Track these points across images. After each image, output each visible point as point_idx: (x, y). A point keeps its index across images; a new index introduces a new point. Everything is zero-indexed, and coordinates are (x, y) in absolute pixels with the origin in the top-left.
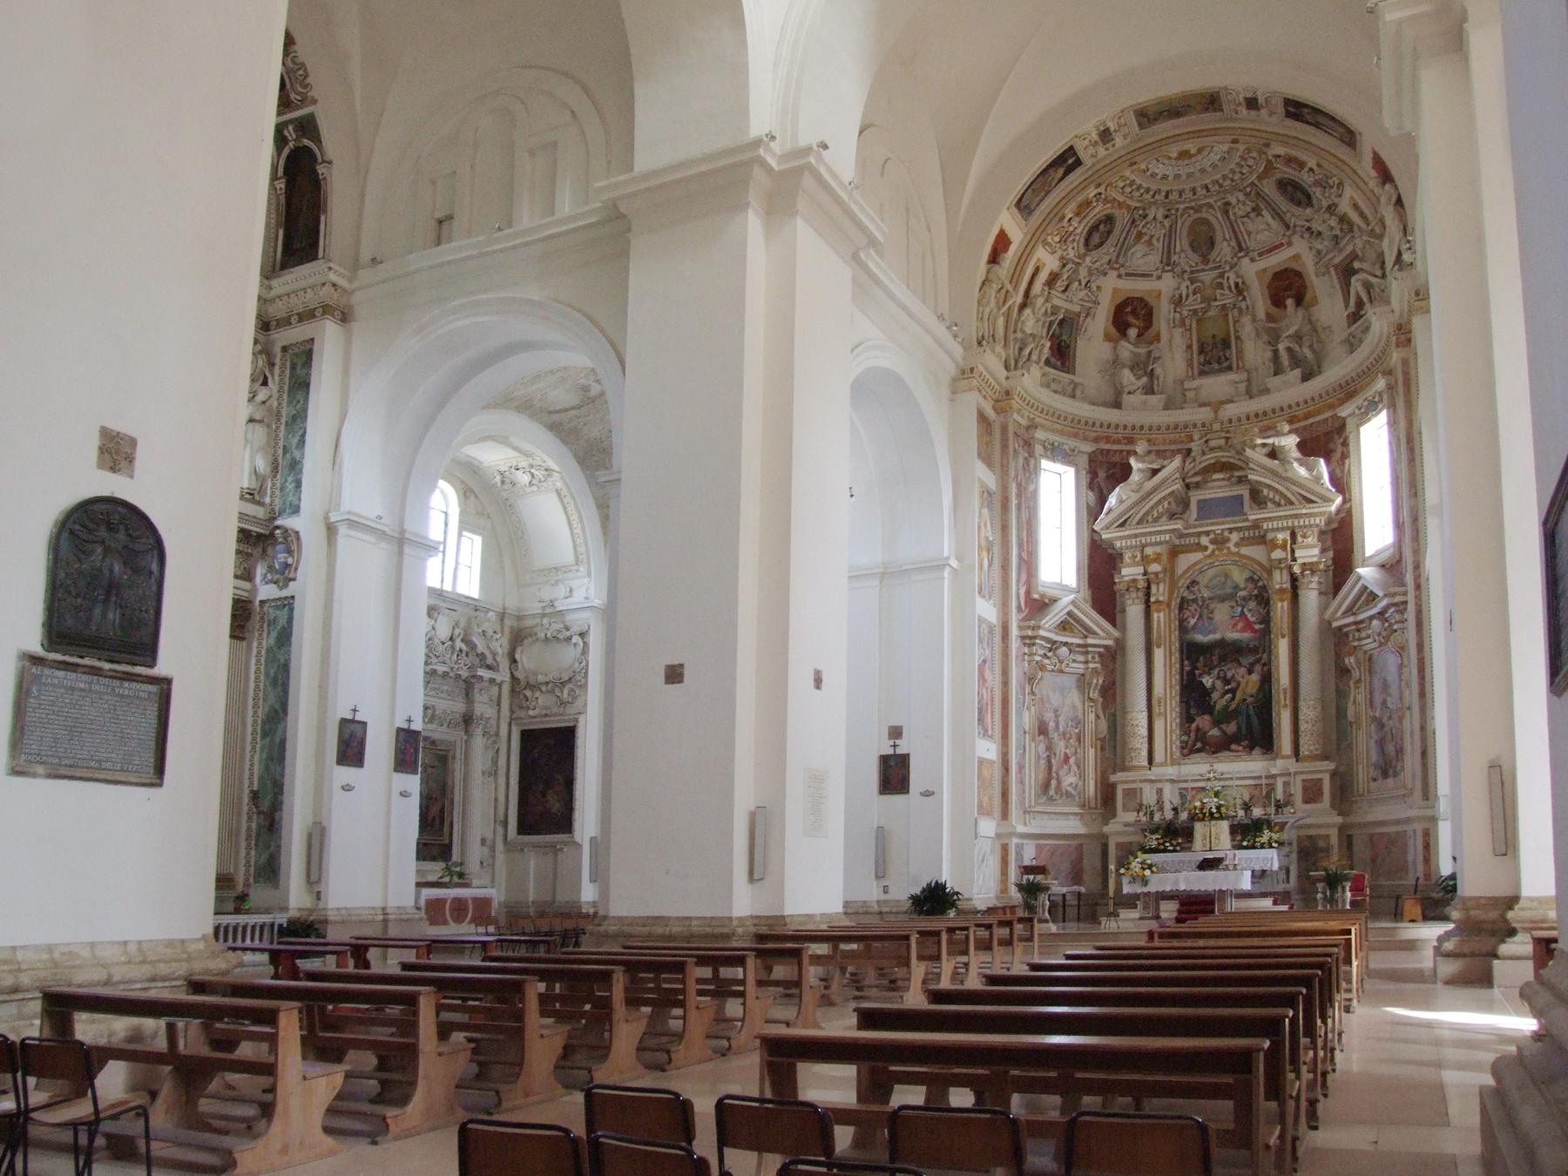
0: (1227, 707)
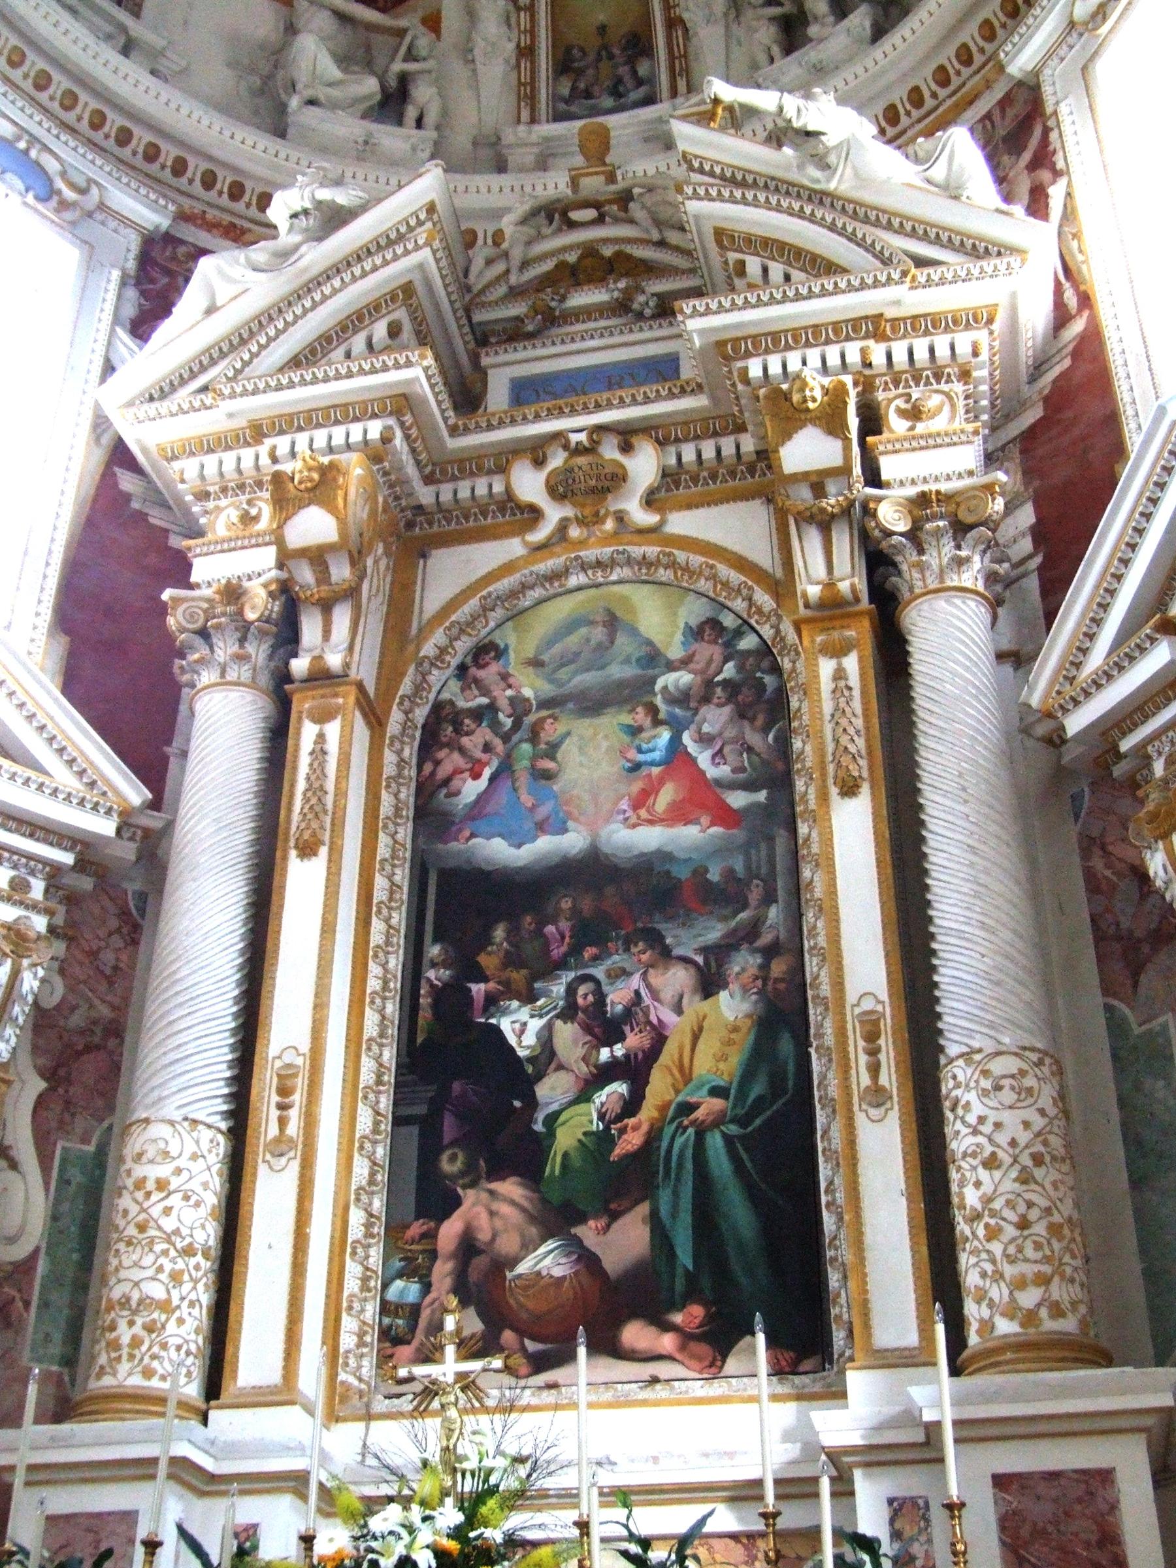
0: (604, 1140)
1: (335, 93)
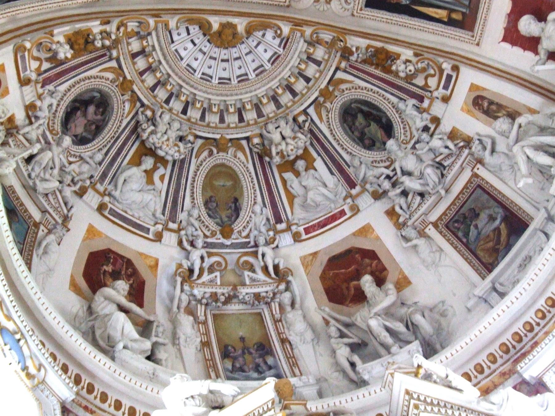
1: (135, 345)
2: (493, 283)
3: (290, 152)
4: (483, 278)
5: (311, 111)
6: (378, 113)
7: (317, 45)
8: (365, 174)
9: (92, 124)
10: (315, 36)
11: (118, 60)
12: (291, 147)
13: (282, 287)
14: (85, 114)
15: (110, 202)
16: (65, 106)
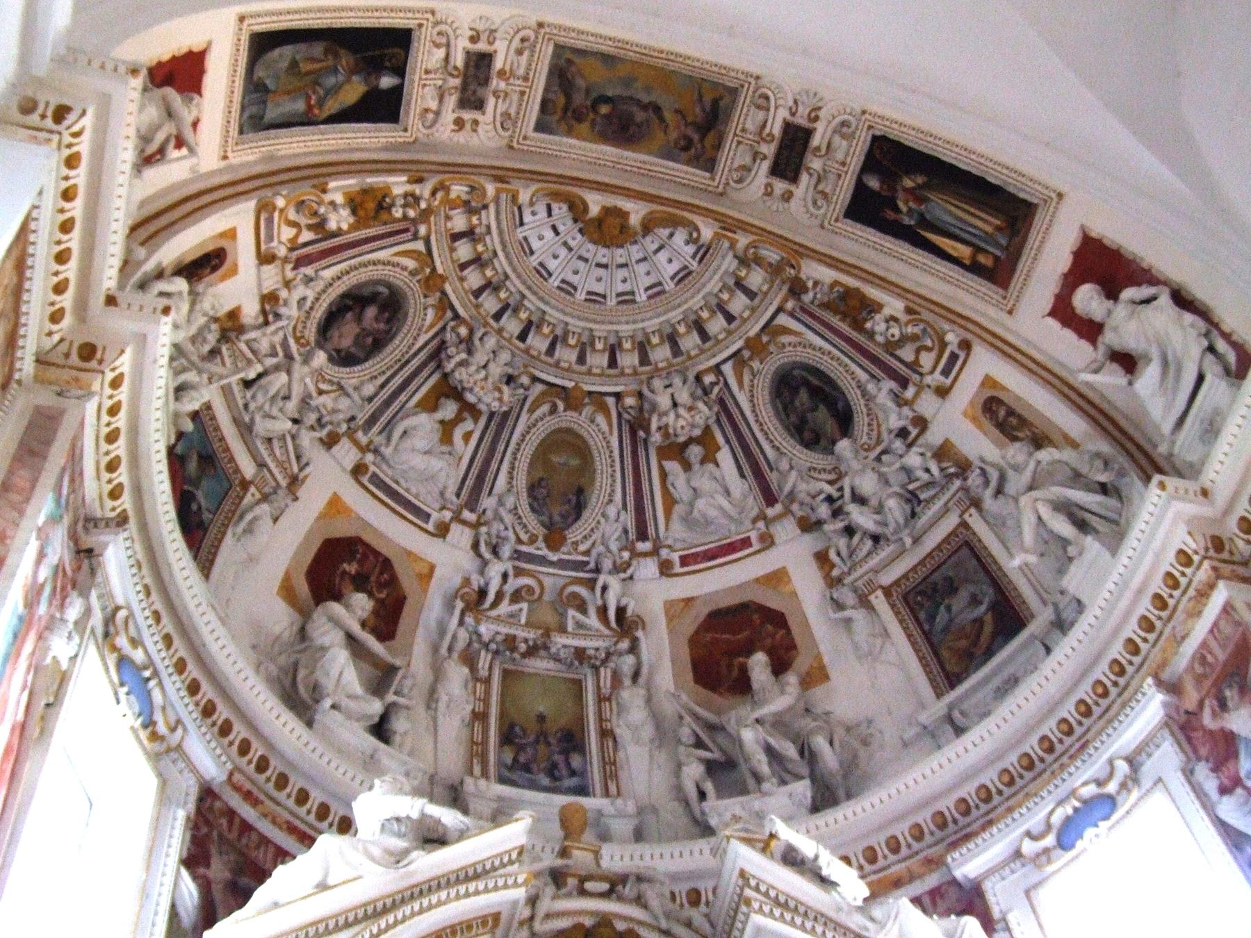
1: (352, 705)
2: (951, 707)
3: (679, 431)
4: (939, 695)
5: (728, 369)
6: (834, 393)
7: (753, 265)
8: (794, 486)
9: (368, 335)
10: (752, 251)
11: (427, 241)
12: (682, 422)
13: (624, 645)
14: (359, 319)
15: (374, 464)
16: (328, 301)
